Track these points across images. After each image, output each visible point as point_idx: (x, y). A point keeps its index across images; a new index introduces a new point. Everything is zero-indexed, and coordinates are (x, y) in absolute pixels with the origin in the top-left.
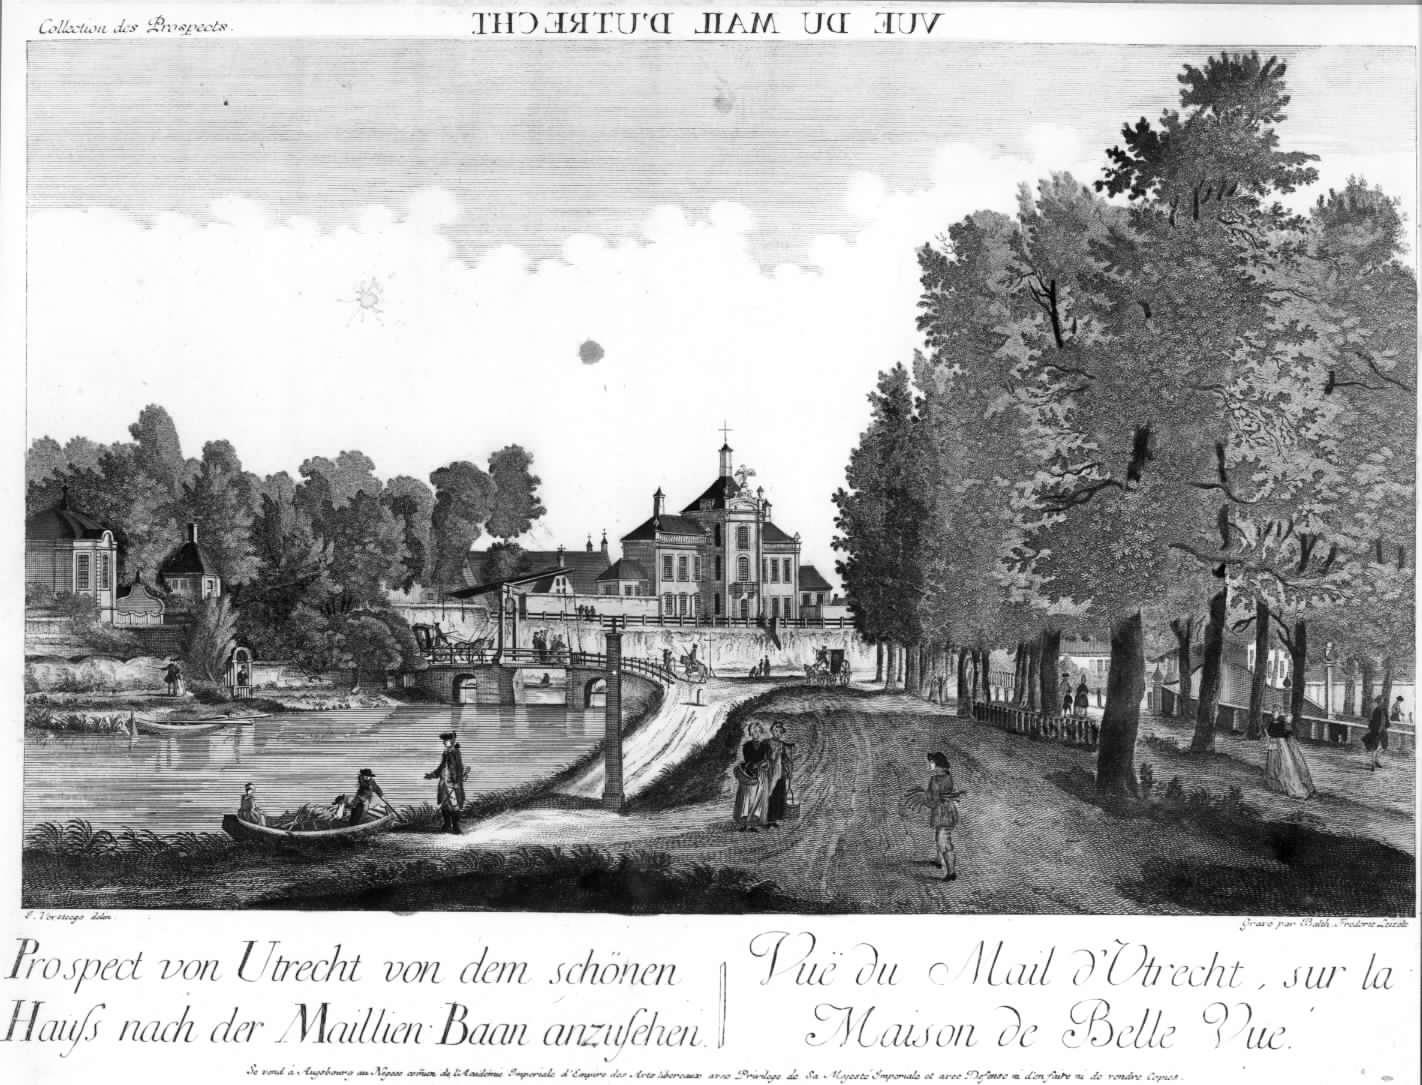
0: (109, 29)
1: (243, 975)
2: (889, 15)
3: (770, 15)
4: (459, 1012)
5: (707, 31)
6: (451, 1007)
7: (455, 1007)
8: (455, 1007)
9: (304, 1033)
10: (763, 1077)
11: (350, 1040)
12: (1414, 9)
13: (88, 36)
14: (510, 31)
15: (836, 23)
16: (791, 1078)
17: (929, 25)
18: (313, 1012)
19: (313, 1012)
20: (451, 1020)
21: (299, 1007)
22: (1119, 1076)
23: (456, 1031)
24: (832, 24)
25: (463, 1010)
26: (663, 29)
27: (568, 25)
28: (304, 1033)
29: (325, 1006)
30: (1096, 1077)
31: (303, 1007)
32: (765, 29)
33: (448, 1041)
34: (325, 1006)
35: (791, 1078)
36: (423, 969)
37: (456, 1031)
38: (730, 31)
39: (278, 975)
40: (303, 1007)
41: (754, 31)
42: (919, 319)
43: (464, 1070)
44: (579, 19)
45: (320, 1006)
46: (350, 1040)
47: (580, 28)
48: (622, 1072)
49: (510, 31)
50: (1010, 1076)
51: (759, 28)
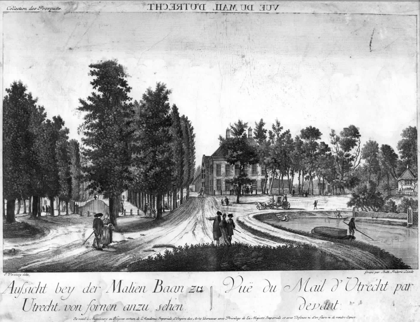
0: (28, 9)
1: (24, 309)
2: (264, 5)
3: (235, 5)
4: (160, 282)
5: (230, 10)
6: (157, 281)
7: (158, 280)
8: (158, 280)
9: (114, 290)
10: (235, 319)
11: (132, 292)
12: (416, 4)
13: (21, 11)
14: (186, 9)
15: (250, 8)
16: (243, 319)
17: (275, 8)
18: (117, 283)
19: (117, 283)
20: (157, 285)
21: (113, 281)
22: (339, 317)
23: (159, 288)
24: (166, 7)
25: (161, 282)
26: (251, 9)
27: (176, 7)
28: (114, 290)
29: (121, 281)
30: (333, 318)
31: (114, 281)
32: (233, 8)
33: (156, 291)
34: (121, 281)
35: (243, 319)
36: (77, 307)
37: (159, 288)
38: (224, 10)
39: (35, 310)
40: (114, 281)
41: (230, 10)
42: (44, 109)
43: (145, 317)
44: (179, 5)
45: (119, 281)
46: (132, 292)
47: (180, 8)
48: (191, 318)
49: (186, 9)
50: (307, 318)
51: (232, 9)
